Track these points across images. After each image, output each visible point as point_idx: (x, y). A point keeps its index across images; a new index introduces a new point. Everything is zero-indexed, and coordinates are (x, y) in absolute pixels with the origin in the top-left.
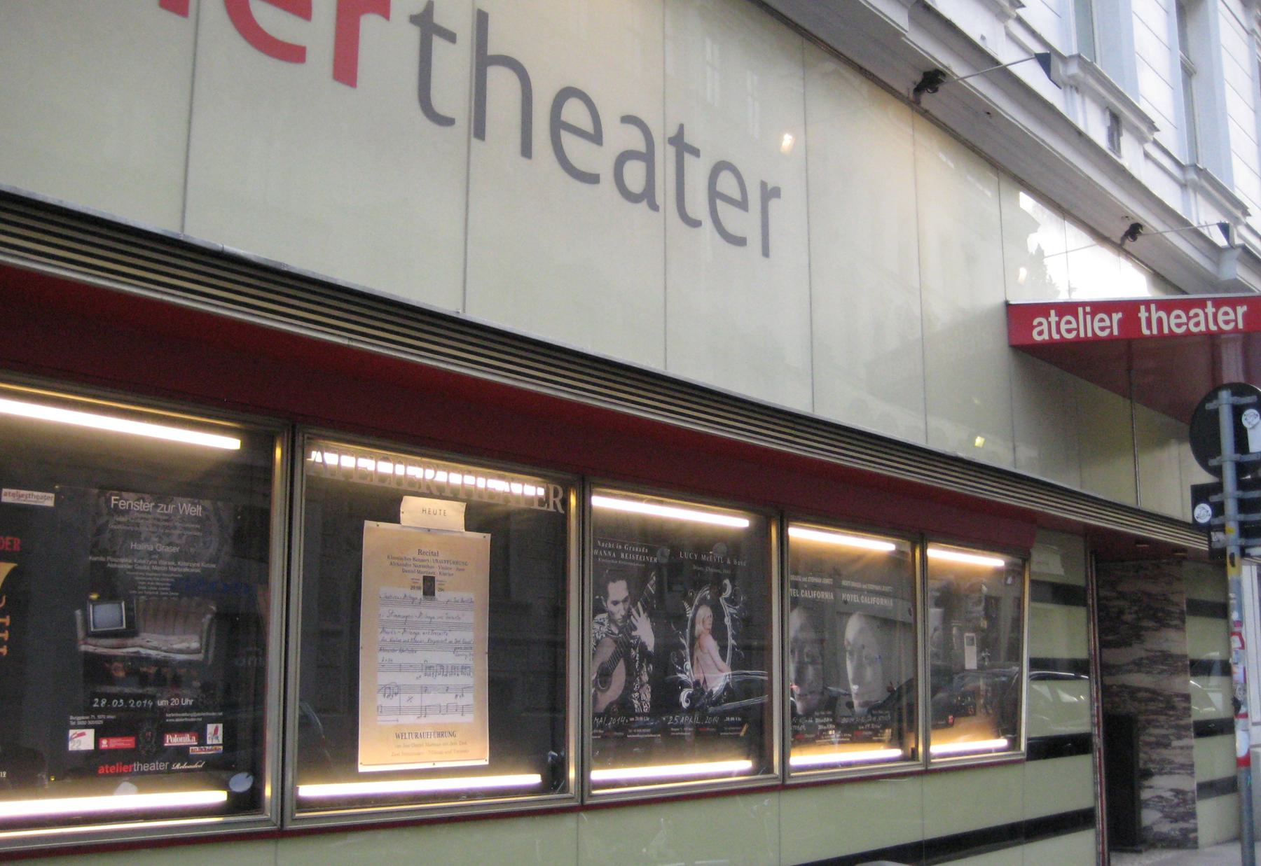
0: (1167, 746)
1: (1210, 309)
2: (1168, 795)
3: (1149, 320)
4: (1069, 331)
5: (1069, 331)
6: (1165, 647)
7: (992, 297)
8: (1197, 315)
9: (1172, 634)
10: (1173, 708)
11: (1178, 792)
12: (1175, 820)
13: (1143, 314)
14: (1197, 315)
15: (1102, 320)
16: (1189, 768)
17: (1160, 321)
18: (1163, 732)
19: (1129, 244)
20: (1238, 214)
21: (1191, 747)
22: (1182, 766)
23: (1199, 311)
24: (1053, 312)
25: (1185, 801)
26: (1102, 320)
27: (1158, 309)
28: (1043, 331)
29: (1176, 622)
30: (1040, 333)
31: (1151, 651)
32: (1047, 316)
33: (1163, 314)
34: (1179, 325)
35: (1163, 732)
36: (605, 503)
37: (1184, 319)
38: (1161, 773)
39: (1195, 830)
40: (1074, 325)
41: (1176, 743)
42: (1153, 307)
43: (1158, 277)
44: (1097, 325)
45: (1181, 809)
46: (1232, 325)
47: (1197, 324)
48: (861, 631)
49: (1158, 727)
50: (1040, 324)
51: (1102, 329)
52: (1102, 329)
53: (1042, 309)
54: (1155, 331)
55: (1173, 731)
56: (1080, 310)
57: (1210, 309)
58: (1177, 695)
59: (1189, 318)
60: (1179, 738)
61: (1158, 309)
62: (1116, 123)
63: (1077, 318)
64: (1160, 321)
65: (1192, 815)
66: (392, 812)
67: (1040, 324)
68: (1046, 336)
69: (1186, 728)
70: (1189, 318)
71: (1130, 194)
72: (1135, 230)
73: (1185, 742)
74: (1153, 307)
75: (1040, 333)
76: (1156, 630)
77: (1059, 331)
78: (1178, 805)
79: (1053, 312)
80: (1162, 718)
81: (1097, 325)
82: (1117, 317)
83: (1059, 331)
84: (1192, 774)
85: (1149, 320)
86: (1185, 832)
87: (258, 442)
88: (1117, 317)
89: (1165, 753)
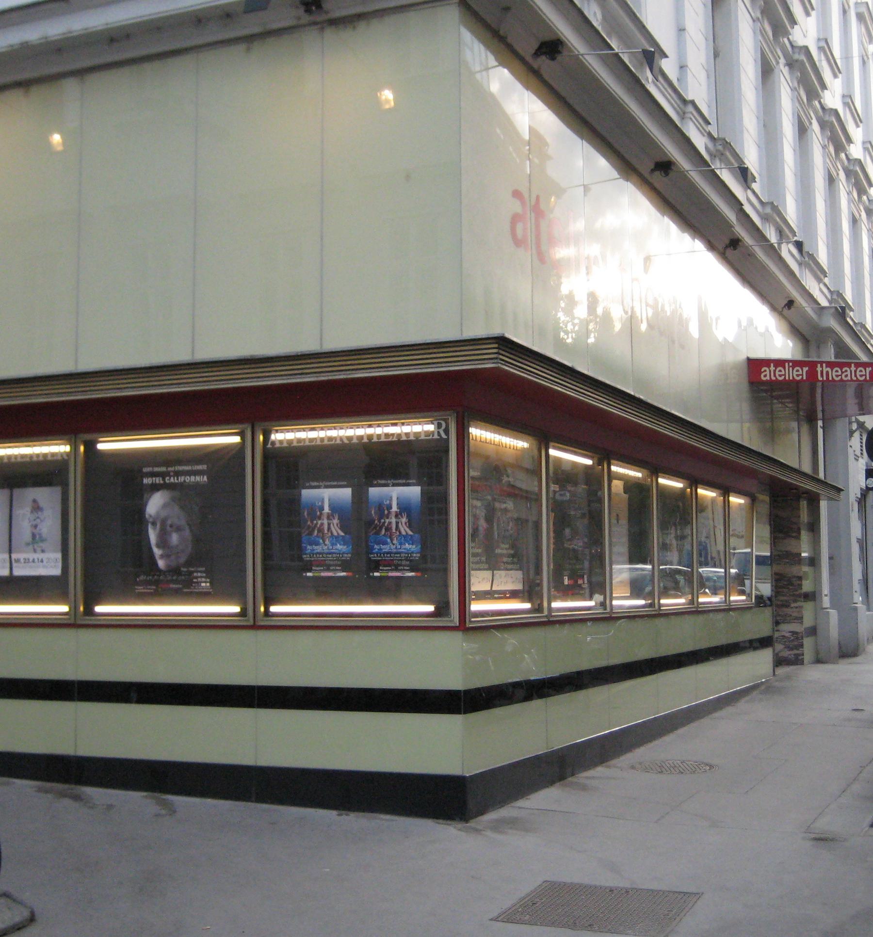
0: (788, 606)
1: (853, 368)
2: (788, 635)
3: (822, 372)
4: (780, 376)
5: (780, 376)
6: (788, 549)
7: (743, 357)
8: (846, 371)
9: (793, 542)
10: (792, 585)
11: (794, 633)
12: (792, 649)
13: (819, 369)
14: (846, 371)
15: (798, 371)
16: (800, 619)
17: (827, 373)
18: (785, 598)
19: (786, 312)
20: (822, 277)
21: (801, 607)
22: (797, 618)
23: (848, 369)
24: (772, 365)
25: (797, 638)
26: (798, 371)
27: (827, 367)
28: (767, 374)
29: (794, 534)
30: (765, 376)
31: (781, 551)
32: (769, 366)
33: (829, 369)
34: (837, 376)
35: (785, 598)
36: (662, 481)
37: (840, 373)
38: (783, 623)
39: (803, 655)
40: (783, 373)
41: (792, 605)
42: (824, 365)
43: (805, 333)
44: (795, 373)
45: (796, 643)
46: (863, 378)
47: (846, 376)
48: (165, 506)
49: (784, 596)
50: (765, 371)
51: (798, 375)
52: (798, 375)
53: (766, 362)
54: (825, 378)
55: (792, 598)
56: (787, 365)
57: (853, 368)
58: (795, 577)
59: (842, 373)
60: (795, 601)
61: (827, 367)
62: (780, 232)
63: (784, 368)
64: (827, 373)
65: (802, 646)
66: (514, 619)
67: (765, 371)
68: (768, 378)
69: (800, 596)
70: (842, 373)
71: (793, 285)
72: (790, 303)
73: (799, 604)
74: (824, 365)
75: (765, 376)
76: (785, 538)
77: (775, 375)
78: (793, 640)
79: (772, 365)
80: (785, 590)
81: (795, 373)
82: (805, 369)
83: (775, 375)
84: (802, 623)
85: (822, 372)
86: (797, 655)
87: (600, 463)
88: (805, 369)
89: (788, 611)
